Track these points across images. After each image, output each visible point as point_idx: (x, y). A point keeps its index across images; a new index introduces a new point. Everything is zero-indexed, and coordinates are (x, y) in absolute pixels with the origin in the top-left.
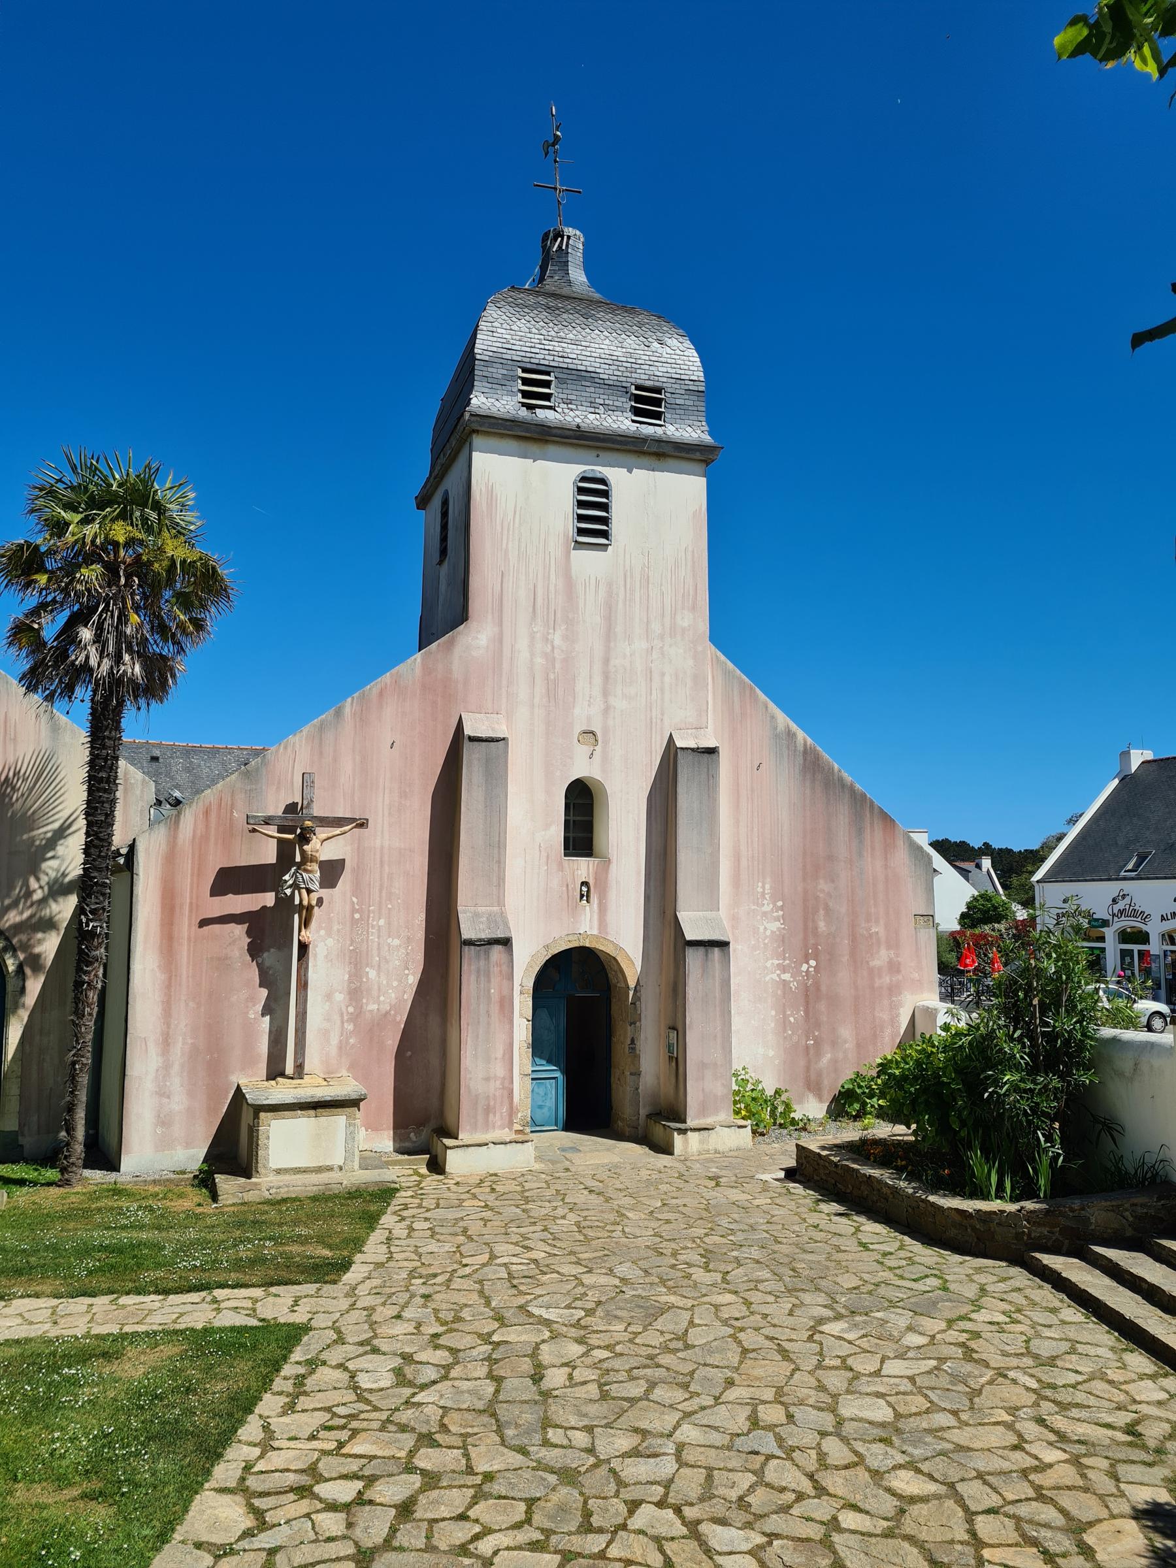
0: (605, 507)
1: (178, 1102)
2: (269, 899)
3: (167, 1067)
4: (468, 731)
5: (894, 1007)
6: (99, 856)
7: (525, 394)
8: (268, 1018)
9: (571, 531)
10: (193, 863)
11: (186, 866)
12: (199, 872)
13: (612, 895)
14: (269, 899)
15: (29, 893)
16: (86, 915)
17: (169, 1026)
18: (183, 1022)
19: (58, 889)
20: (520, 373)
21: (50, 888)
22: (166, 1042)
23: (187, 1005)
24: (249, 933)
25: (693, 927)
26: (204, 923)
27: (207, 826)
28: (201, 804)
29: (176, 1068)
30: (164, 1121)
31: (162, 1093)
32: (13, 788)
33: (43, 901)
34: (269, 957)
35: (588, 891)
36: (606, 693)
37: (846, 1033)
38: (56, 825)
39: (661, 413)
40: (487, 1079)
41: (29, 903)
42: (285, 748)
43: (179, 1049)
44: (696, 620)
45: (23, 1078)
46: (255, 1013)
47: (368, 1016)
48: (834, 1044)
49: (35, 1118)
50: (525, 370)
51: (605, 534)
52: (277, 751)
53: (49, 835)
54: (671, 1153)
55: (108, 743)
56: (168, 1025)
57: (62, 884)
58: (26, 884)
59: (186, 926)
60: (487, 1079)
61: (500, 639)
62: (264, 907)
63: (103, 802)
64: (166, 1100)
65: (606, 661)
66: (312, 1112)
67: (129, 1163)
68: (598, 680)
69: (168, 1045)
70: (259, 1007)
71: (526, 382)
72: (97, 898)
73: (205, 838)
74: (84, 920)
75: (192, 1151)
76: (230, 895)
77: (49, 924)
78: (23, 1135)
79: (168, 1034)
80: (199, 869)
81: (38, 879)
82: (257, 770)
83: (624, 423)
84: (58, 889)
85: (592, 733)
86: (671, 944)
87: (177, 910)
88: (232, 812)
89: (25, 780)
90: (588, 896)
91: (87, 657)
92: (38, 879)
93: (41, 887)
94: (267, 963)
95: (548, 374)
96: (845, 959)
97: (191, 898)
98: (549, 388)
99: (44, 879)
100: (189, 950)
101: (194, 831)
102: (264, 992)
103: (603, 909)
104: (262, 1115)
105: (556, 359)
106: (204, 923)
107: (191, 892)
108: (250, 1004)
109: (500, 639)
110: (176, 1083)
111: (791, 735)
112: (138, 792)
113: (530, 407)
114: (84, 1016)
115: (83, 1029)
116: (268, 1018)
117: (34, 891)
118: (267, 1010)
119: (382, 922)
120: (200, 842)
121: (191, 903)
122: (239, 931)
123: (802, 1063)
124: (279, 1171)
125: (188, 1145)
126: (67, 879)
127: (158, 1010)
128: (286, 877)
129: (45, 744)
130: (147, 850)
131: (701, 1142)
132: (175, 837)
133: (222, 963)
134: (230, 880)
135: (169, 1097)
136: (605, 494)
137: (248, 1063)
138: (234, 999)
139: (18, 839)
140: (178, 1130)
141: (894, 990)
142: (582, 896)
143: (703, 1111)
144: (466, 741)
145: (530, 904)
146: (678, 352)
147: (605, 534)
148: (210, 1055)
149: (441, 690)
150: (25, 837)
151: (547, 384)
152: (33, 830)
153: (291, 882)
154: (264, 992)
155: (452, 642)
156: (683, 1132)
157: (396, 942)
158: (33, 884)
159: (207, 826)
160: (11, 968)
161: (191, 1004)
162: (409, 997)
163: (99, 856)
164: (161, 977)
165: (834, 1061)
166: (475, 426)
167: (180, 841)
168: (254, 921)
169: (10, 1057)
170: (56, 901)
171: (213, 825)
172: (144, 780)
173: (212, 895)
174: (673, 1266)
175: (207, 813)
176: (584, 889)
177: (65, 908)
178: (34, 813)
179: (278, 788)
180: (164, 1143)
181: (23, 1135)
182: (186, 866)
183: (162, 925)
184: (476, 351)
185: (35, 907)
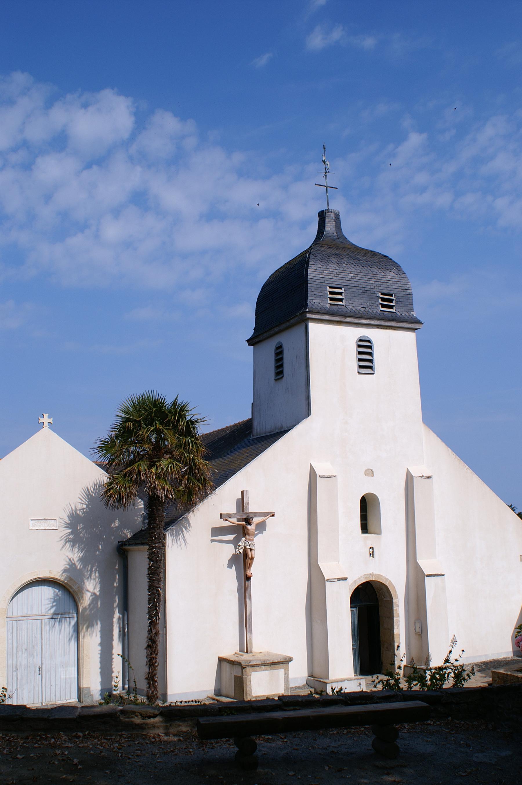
0: (370, 354)
4: (319, 473)
9: (356, 367)
20: (380, 301)
25: (427, 565)
35: (373, 552)
39: (393, 306)
51: (371, 368)
71: (383, 299)
85: (371, 470)
90: (373, 554)
95: (341, 288)
98: (392, 302)
105: (388, 289)
128: (240, 544)
136: (370, 347)
142: (370, 554)
144: (318, 477)
145: (349, 562)
146: (399, 276)
147: (371, 368)
151: (341, 294)
173: (219, 658)
176: (371, 550)
184: (308, 279)
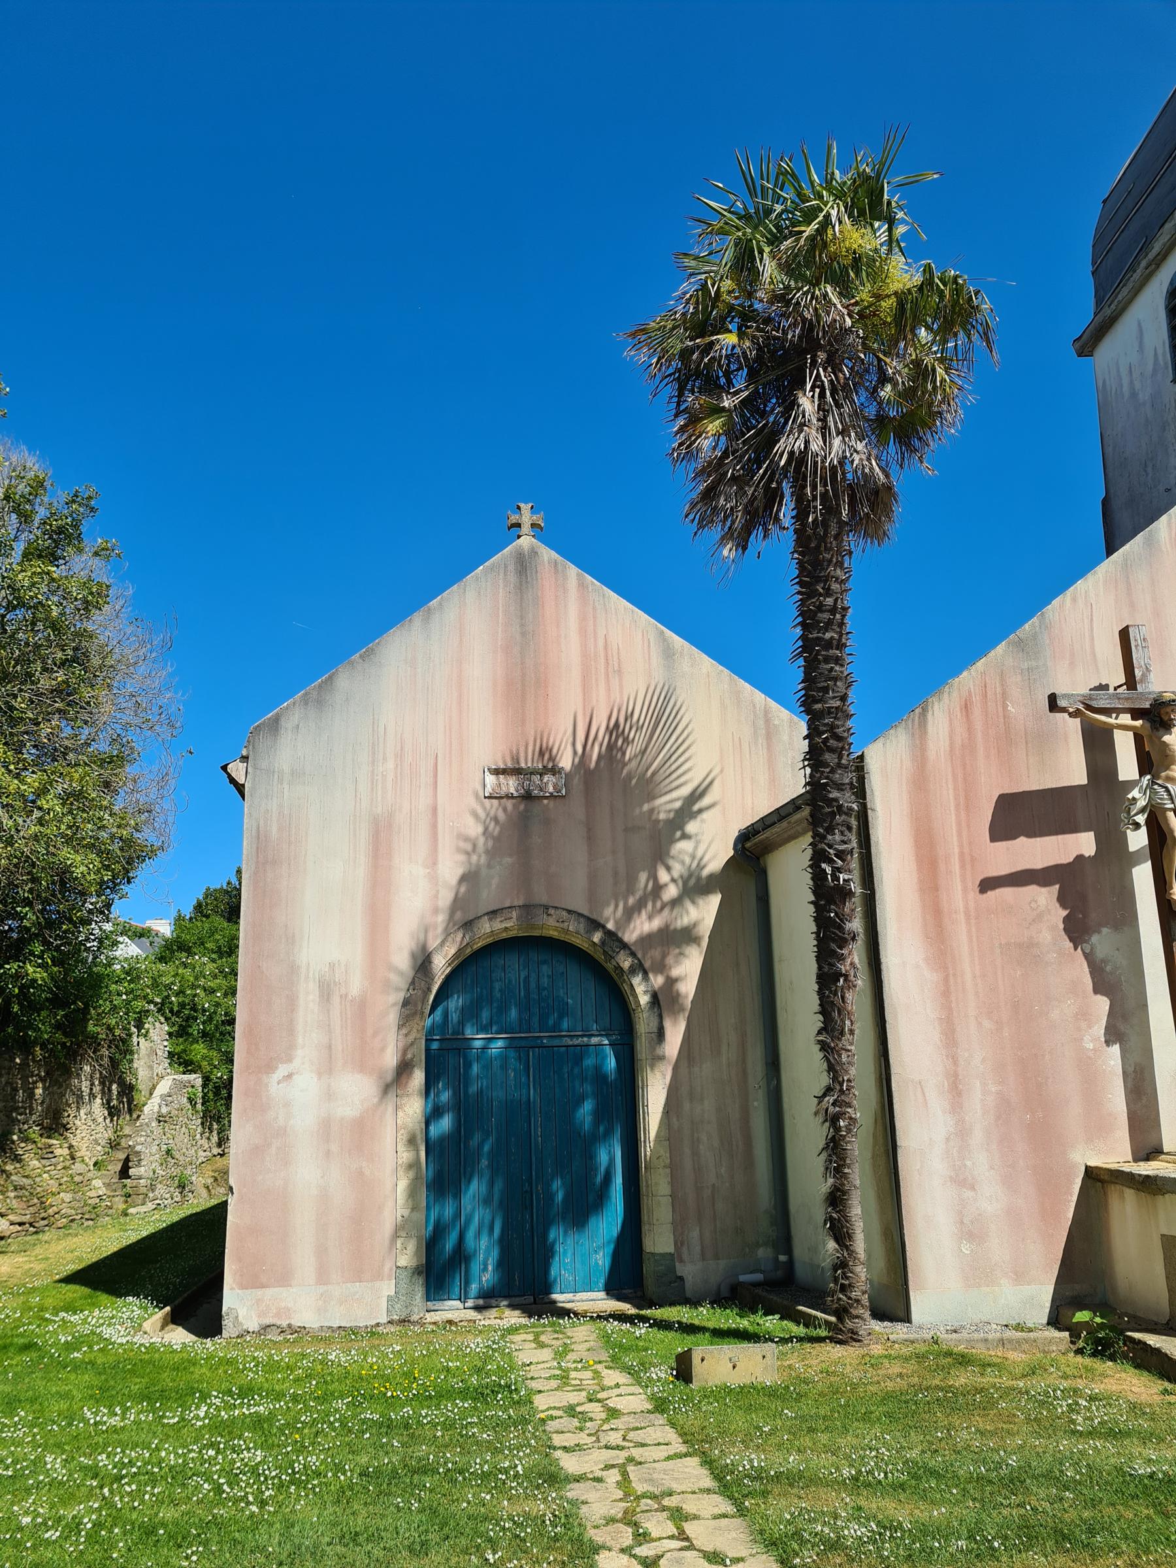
1: (990, 1198)
2: (1085, 843)
3: (962, 1132)
6: (839, 765)
8: (1116, 1049)
10: (955, 789)
11: (946, 794)
12: (967, 802)
14: (1085, 843)
15: (658, 888)
16: (830, 861)
17: (955, 1062)
18: (977, 1056)
19: (695, 887)
21: (685, 883)
22: (955, 1089)
23: (980, 1024)
24: (1062, 900)
26: (987, 885)
27: (970, 729)
28: (955, 694)
29: (977, 1136)
30: (971, 1231)
31: (962, 1181)
32: (626, 740)
33: (675, 903)
34: (1103, 941)
38: (685, 791)
41: (659, 904)
42: (1074, 600)
45: (674, 1168)
46: (1094, 1040)
49: (695, 1234)
52: (1062, 606)
53: (678, 804)
55: (835, 586)
56: (955, 1060)
57: (699, 878)
58: (654, 876)
59: (959, 893)
62: (1080, 858)
63: (835, 679)
64: (969, 1194)
67: (921, 1305)
69: (959, 1094)
70: (1099, 1030)
72: (842, 833)
73: (969, 747)
74: (829, 870)
75: (1028, 1290)
76: (1022, 839)
77: (687, 936)
78: (681, 1261)
79: (956, 1075)
80: (967, 798)
81: (668, 869)
82: (1035, 637)
84: (695, 887)
87: (942, 867)
88: (1005, 707)
89: (639, 728)
91: (807, 442)
92: (668, 869)
93: (673, 880)
94: (1100, 954)
97: (961, 846)
99: (678, 869)
100: (969, 931)
101: (951, 738)
102: (1103, 1004)
106: (987, 885)
107: (960, 835)
108: (1084, 1025)
110: (982, 1163)
112: (785, 738)
114: (842, 1033)
115: (844, 1058)
116: (1116, 1049)
117: (666, 885)
118: (1113, 1034)
120: (963, 754)
121: (962, 854)
122: (1045, 897)
125: (1019, 1276)
126: (705, 872)
129: (658, 676)
133: (1025, 953)
134: (1017, 815)
135: (973, 1188)
137: (1098, 1129)
138: (1055, 1015)
139: (637, 811)
140: (998, 1249)
148: (1031, 1114)
150: (646, 807)
152: (654, 798)
153: (1142, 803)
154: (1103, 1004)
158: (663, 876)
159: (970, 729)
160: (644, 1000)
161: (987, 1024)
163: (839, 765)
164: (931, 976)
167: (931, 754)
168: (1065, 879)
169: (653, 1134)
170: (693, 902)
171: (978, 725)
172: (791, 721)
173: (993, 839)
175: (967, 707)
177: (704, 913)
178: (654, 774)
179: (1072, 664)
180: (978, 1273)
181: (681, 1261)
182: (946, 794)
183: (922, 890)
185: (666, 911)
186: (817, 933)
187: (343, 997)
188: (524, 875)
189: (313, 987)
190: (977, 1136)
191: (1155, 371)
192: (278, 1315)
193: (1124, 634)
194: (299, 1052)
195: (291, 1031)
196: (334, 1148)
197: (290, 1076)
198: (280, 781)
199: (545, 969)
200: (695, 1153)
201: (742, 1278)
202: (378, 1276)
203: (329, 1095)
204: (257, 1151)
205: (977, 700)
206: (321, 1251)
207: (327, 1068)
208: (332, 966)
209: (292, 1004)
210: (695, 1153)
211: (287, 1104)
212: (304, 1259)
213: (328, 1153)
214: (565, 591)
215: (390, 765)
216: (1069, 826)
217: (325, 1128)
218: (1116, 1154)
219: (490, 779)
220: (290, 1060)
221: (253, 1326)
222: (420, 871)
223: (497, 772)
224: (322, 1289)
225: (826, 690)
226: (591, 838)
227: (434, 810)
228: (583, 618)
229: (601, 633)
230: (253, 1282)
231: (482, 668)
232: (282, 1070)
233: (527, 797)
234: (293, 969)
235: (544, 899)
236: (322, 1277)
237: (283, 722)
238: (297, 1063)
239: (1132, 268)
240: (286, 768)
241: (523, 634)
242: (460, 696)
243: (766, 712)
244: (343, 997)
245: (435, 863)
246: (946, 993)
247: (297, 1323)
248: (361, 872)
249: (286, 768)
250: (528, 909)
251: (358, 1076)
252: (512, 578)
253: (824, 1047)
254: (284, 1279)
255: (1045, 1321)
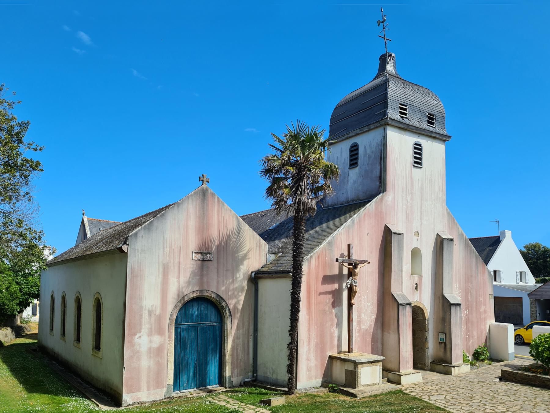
1: (313, 363)
3: (309, 350)
5: (485, 325)
7: (401, 113)
13: (423, 288)
18: (313, 334)
29: (312, 350)
30: (309, 370)
31: (308, 360)
36: (421, 219)
37: (475, 333)
40: (406, 352)
43: (313, 343)
44: (442, 195)
47: (362, 330)
48: (472, 337)
49: (236, 371)
50: (401, 104)
54: (451, 375)
60: (406, 352)
61: (394, 198)
65: (421, 208)
66: (371, 364)
68: (419, 214)
73: (318, 266)
83: (424, 125)
86: (445, 306)
95: (406, 106)
96: (474, 309)
103: (420, 292)
104: (359, 366)
109: (394, 198)
110: (312, 356)
111: (462, 235)
113: (402, 117)
119: (366, 297)
123: (466, 343)
124: (363, 386)
125: (316, 378)
127: (307, 329)
130: (309, 273)
131: (459, 370)
132: (310, 266)
136: (420, 150)
137: (332, 347)
140: (313, 373)
141: (485, 319)
143: (456, 361)
148: (321, 346)
149: (379, 215)
155: (382, 199)
156: (454, 367)
157: (369, 304)
161: (316, 327)
162: (373, 323)
164: (307, 317)
165: (473, 342)
166: (390, 122)
174: (485, 405)
175: (318, 257)
180: (310, 378)
186: (291, 310)
187: (155, 315)
188: (201, 283)
189: (147, 312)
190: (312, 350)
191: (344, 163)
192: (137, 399)
193: (349, 246)
194: (143, 330)
195: (141, 324)
196: (152, 355)
197: (140, 337)
198: (138, 252)
199: (202, 306)
200: (237, 352)
201: (246, 380)
202: (163, 387)
203: (151, 342)
204: (131, 357)
205: (320, 255)
206: (148, 382)
207: (150, 334)
208: (152, 306)
209: (141, 316)
210: (237, 352)
211: (140, 344)
212: (144, 385)
213: (150, 357)
214: (214, 202)
215: (168, 249)
216: (333, 283)
217: (150, 350)
218: (334, 353)
219: (194, 254)
220: (140, 332)
221: (131, 403)
222: (175, 280)
223: (195, 253)
224: (148, 392)
225: (299, 255)
226: (218, 272)
227: (180, 263)
228: (218, 211)
229: (223, 216)
230: (130, 392)
231: (192, 223)
232: (138, 335)
233: (203, 260)
234: (141, 307)
235: (206, 289)
236: (148, 389)
237: (138, 234)
238: (142, 333)
239: (343, 136)
240: (140, 249)
241: (203, 214)
242: (187, 230)
243: (260, 241)
244: (155, 315)
245: (179, 278)
246: (309, 321)
247: (142, 401)
248: (160, 280)
249: (140, 249)
250: (201, 291)
251: (158, 336)
252: (201, 196)
253: (290, 335)
254: (139, 390)
255: (320, 385)
